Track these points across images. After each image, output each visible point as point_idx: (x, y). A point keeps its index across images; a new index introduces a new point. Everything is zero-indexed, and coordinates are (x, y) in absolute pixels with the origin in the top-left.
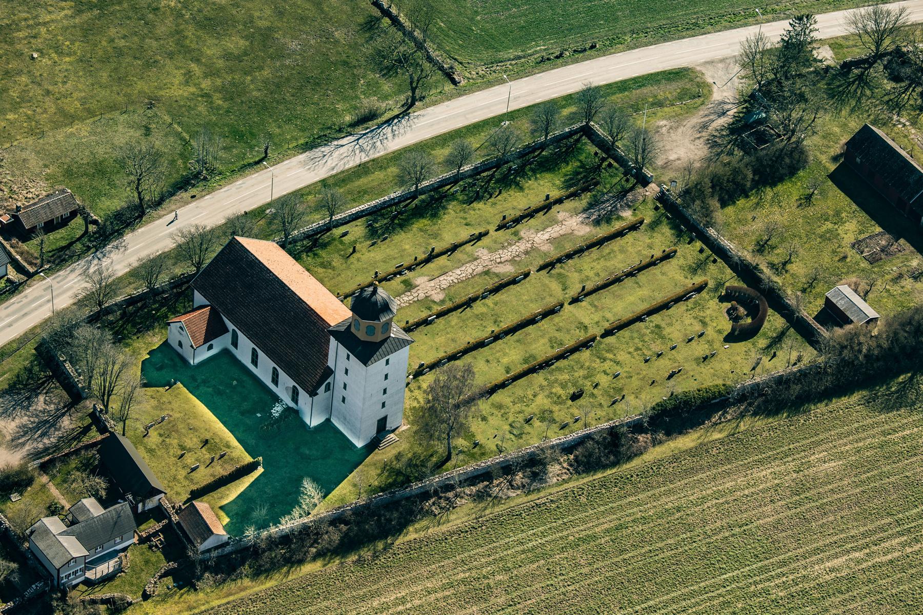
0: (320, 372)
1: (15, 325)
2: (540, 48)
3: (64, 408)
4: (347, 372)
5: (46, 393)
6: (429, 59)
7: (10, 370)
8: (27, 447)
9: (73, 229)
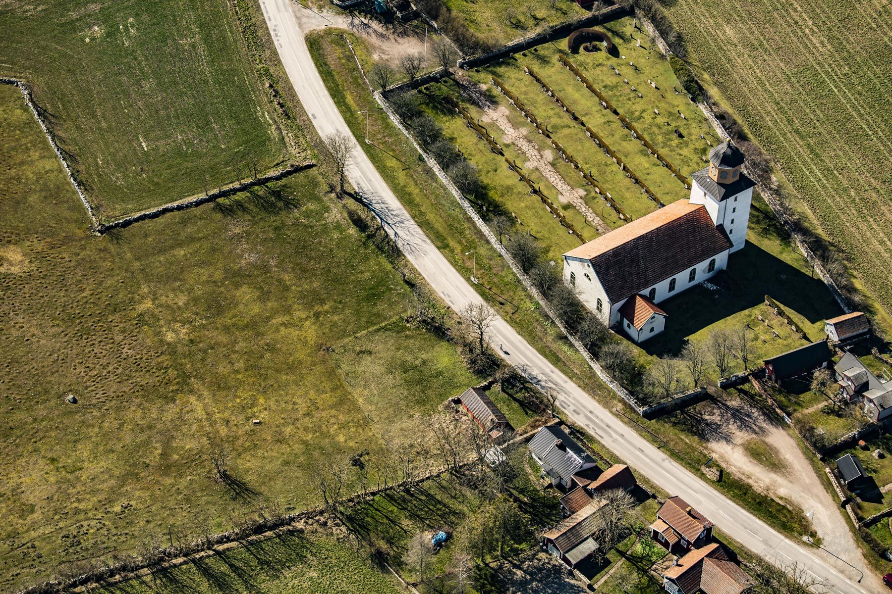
0: (718, 234)
1: (621, 432)
2: (266, 114)
3: (716, 404)
4: (734, 210)
5: (701, 414)
6: (278, 178)
7: (675, 434)
8: (764, 425)
9: (496, 399)
